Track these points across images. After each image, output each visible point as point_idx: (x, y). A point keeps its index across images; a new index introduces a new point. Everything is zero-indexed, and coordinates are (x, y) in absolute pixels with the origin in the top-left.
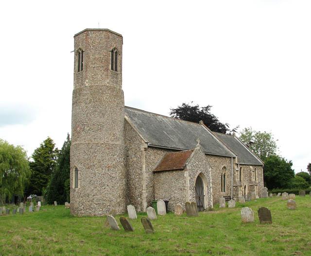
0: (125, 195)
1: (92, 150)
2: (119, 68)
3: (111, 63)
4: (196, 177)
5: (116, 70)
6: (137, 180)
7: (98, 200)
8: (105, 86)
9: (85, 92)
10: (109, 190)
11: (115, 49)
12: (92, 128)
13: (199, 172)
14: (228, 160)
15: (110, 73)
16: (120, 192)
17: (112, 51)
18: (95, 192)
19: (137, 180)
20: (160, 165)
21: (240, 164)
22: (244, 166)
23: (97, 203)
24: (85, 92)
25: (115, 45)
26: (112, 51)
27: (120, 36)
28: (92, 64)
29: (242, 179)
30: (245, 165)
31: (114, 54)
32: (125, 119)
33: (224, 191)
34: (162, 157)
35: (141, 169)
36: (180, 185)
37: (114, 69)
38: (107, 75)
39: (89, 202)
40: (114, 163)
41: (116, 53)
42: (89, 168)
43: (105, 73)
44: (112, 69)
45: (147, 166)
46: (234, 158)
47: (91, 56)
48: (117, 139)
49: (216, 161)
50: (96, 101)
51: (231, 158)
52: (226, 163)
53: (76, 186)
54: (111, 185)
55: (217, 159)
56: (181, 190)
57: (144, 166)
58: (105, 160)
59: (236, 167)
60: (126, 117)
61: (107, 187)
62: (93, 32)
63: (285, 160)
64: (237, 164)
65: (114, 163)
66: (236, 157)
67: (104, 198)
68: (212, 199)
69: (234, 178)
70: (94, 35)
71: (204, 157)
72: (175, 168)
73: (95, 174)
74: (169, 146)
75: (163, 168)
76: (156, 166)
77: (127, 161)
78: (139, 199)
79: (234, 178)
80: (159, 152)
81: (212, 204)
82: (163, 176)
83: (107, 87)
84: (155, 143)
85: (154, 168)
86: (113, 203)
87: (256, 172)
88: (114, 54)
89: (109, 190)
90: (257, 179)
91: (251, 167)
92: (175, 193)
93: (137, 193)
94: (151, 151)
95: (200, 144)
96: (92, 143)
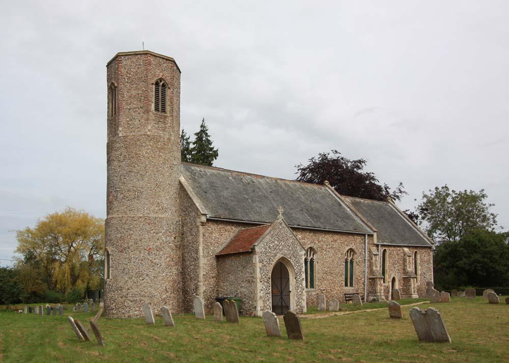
0: (177, 288)
1: (126, 227)
2: (168, 108)
3: (154, 101)
4: (274, 263)
5: (164, 111)
6: (192, 267)
7: (134, 295)
8: (144, 135)
9: (118, 145)
10: (149, 281)
11: (161, 80)
12: (127, 195)
13: (279, 256)
14: (359, 239)
15: (152, 116)
16: (168, 285)
17: (157, 84)
18: (130, 284)
19: (192, 267)
20: (228, 246)
21: (382, 246)
22: (392, 249)
23: (131, 299)
24: (118, 145)
25: (161, 74)
26: (157, 84)
27: (114, 65)
28: (127, 104)
29: (387, 268)
30: (394, 246)
31: (160, 88)
32: (180, 183)
33: (351, 285)
34: (232, 235)
35: (197, 251)
36: (247, 275)
37: (160, 110)
38: (148, 119)
39: (121, 298)
40: (158, 244)
41: (163, 85)
42: (122, 251)
43: (145, 116)
44: (157, 109)
45: (207, 247)
46: (371, 236)
47: (126, 92)
48: (164, 210)
49: (335, 241)
50: (133, 157)
51: (364, 235)
52: (355, 243)
53: (108, 277)
54: (152, 275)
55: (336, 237)
56: (249, 282)
57: (201, 248)
58: (143, 240)
59: (374, 249)
60: (183, 179)
61: (147, 278)
62: (127, 57)
63: (37, 227)
64: (377, 246)
65: (158, 244)
66: (375, 235)
67: (143, 293)
68: (305, 298)
69: (371, 265)
70: (129, 62)
71: (288, 232)
72: (241, 251)
73: (130, 259)
74: (246, 219)
75: (229, 251)
76: (221, 248)
77: (182, 240)
78: (194, 294)
79: (371, 265)
80: (229, 227)
81: (304, 304)
82: (228, 262)
83: (148, 136)
84: (223, 214)
85: (218, 250)
86: (156, 300)
87: (418, 257)
88: (160, 88)
89: (149, 281)
90: (419, 267)
91: (406, 249)
92: (242, 287)
93: (193, 287)
94: (212, 227)
95: (282, 214)
96: (126, 216)
